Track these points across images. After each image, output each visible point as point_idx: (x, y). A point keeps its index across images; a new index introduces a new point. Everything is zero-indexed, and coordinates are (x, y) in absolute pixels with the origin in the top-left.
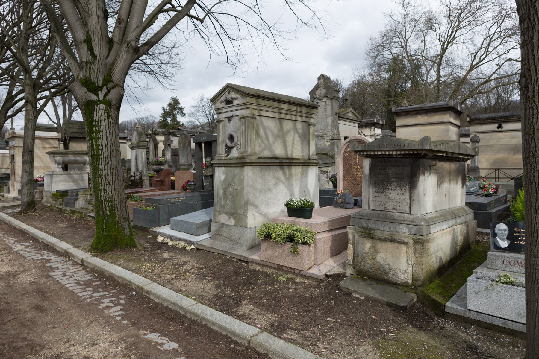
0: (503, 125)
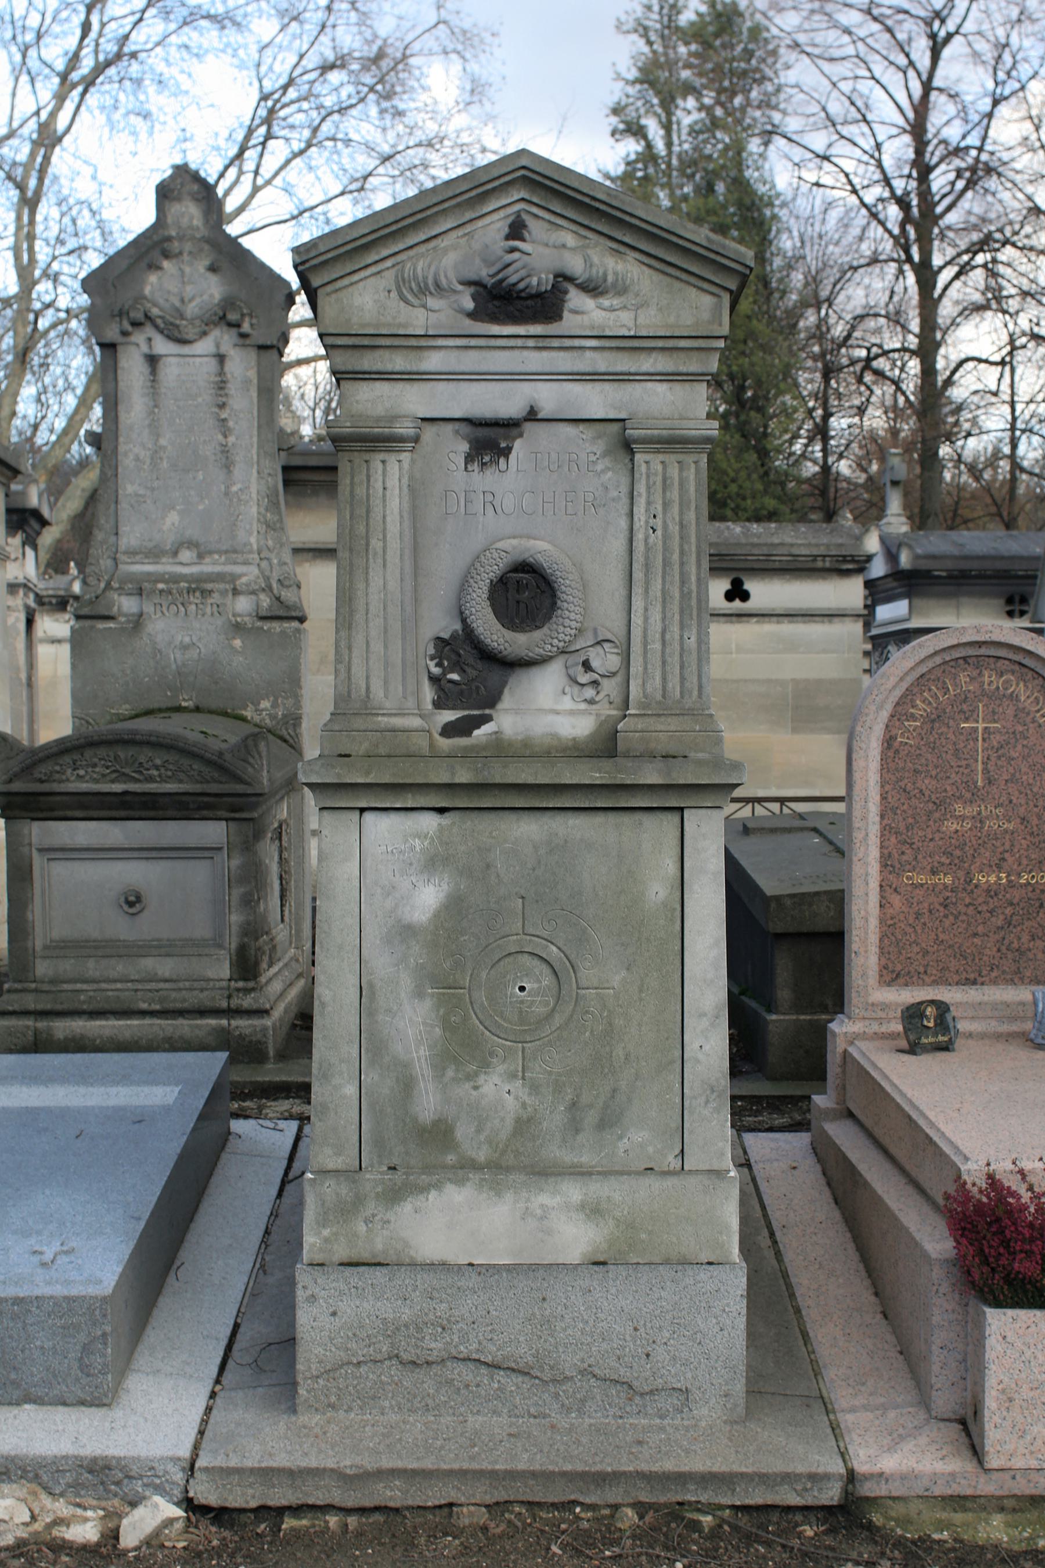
0: (750, 585)
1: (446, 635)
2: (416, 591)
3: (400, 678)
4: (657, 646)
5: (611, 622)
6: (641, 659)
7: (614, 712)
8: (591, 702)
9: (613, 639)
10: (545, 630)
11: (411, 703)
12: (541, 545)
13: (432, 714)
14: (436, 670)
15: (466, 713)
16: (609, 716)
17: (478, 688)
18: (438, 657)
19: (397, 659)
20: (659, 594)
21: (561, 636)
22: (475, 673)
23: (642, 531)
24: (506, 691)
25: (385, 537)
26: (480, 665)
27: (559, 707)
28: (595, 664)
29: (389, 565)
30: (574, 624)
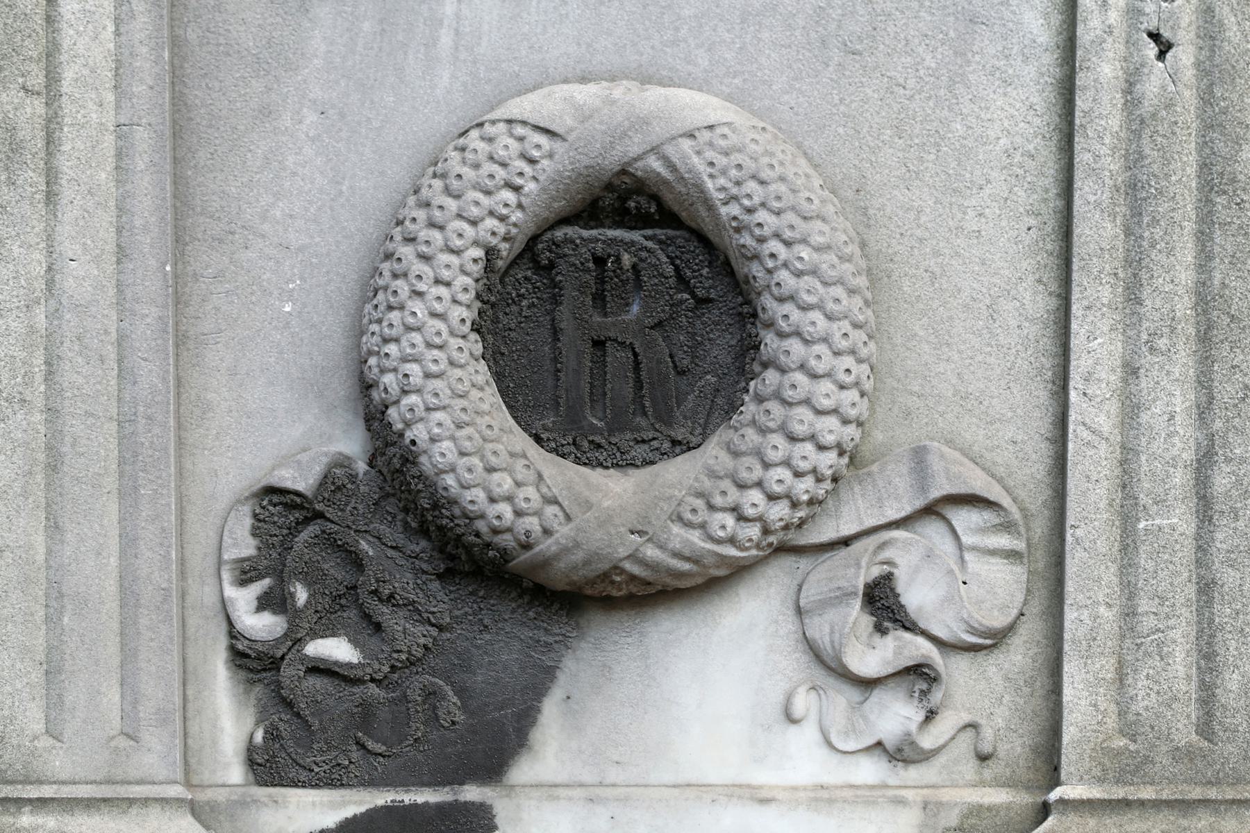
1: (302, 480)
2: (179, 301)
3: (111, 651)
4: (1179, 520)
5: (996, 436)
6: (1109, 575)
7: (998, 797)
8: (901, 753)
9: (994, 492)
10: (713, 452)
11: (154, 758)
12: (695, 105)
13: (243, 803)
14: (262, 625)
15: (382, 798)
16: (977, 811)
17: (431, 694)
18: (269, 570)
19: (96, 568)
20: (1184, 306)
21: (779, 477)
22: (420, 634)
23: (1114, 48)
24: (551, 709)
25: (52, 78)
26: (440, 601)
27: (761, 776)
28: (917, 595)
29: (67, 192)
30: (830, 430)
